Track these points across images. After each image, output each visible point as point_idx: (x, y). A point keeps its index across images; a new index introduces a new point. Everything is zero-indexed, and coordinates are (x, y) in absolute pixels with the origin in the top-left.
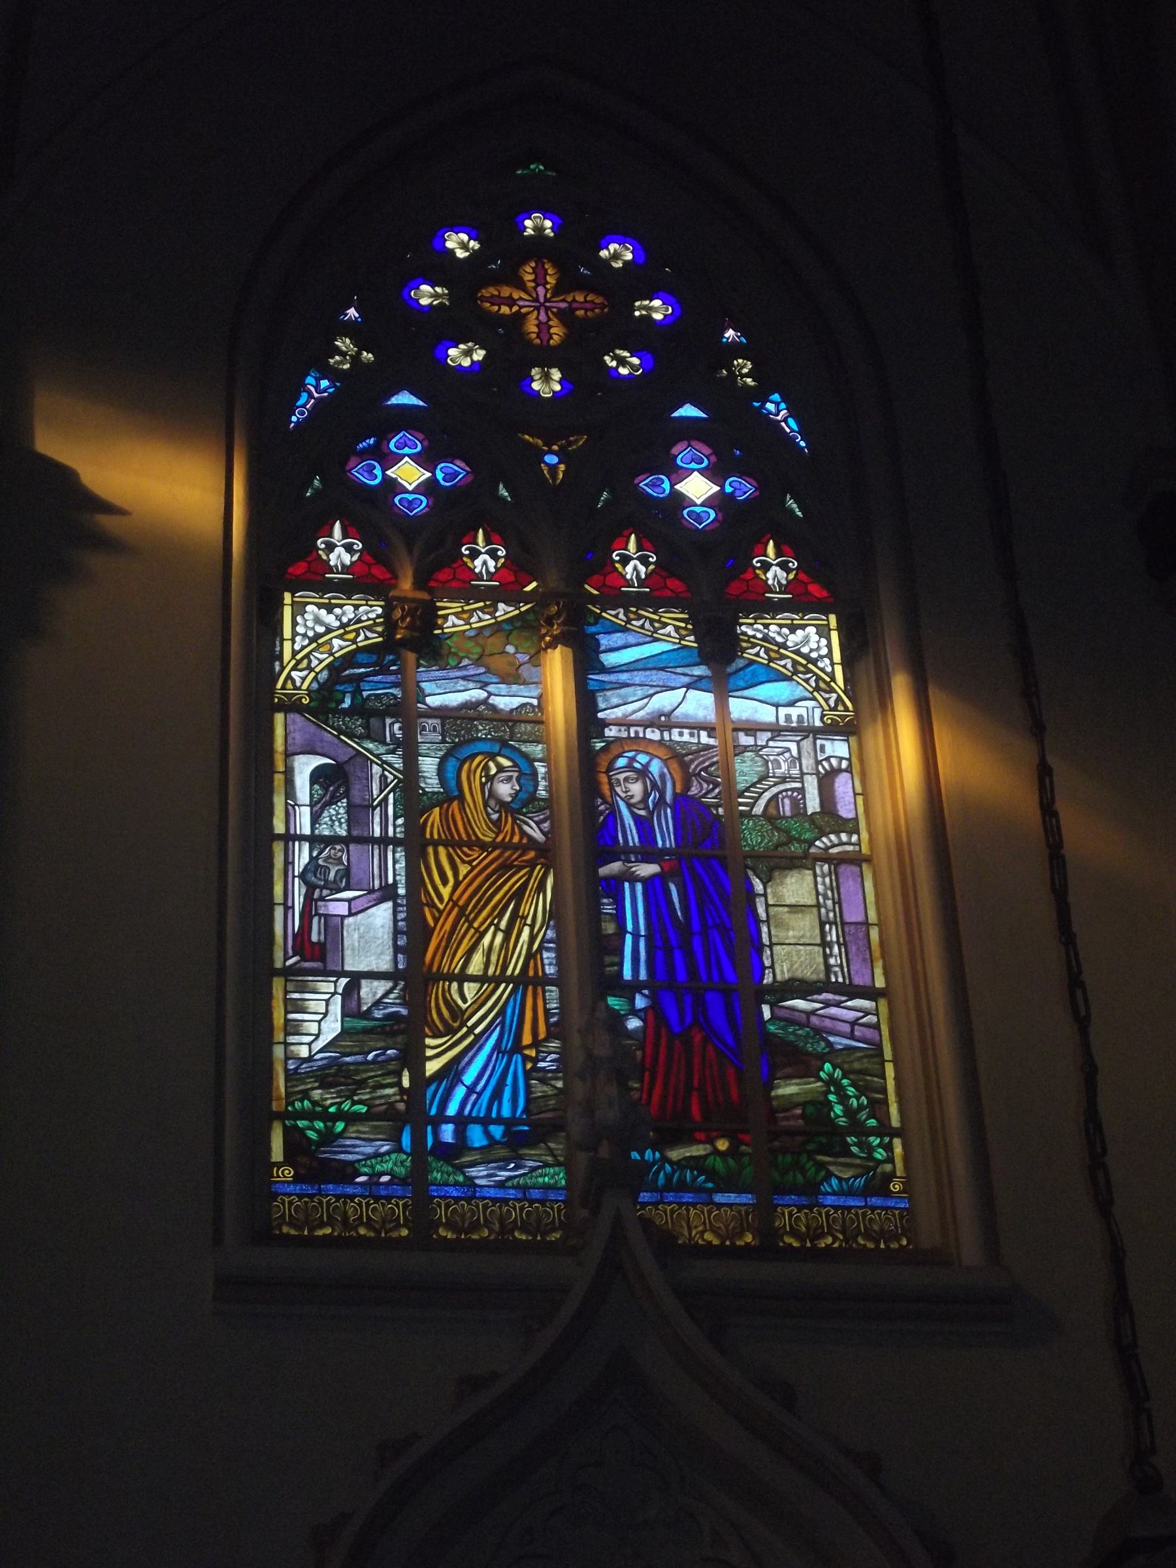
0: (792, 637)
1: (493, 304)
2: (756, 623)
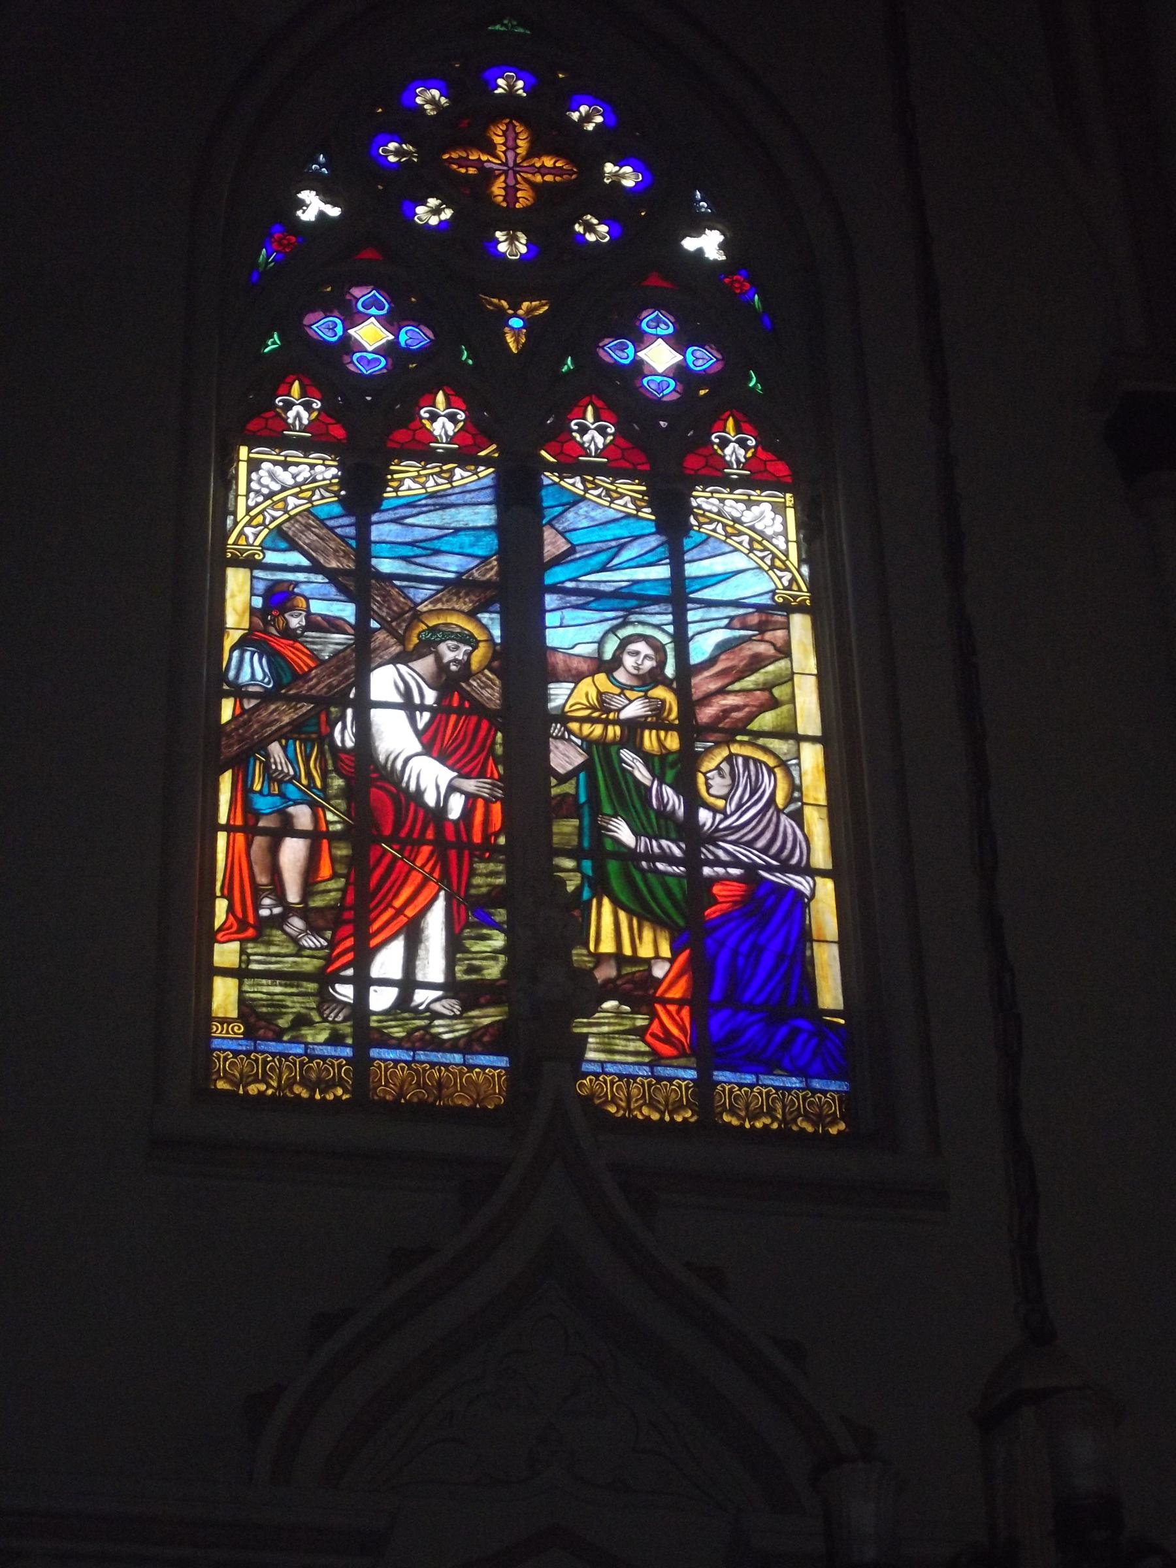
0: (746, 513)
1: (460, 166)
2: (712, 497)
